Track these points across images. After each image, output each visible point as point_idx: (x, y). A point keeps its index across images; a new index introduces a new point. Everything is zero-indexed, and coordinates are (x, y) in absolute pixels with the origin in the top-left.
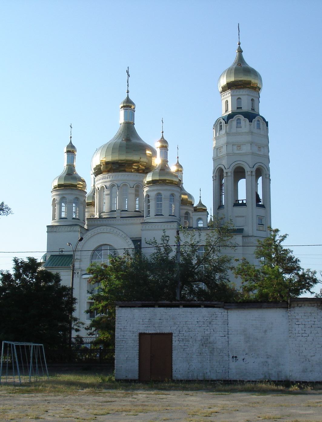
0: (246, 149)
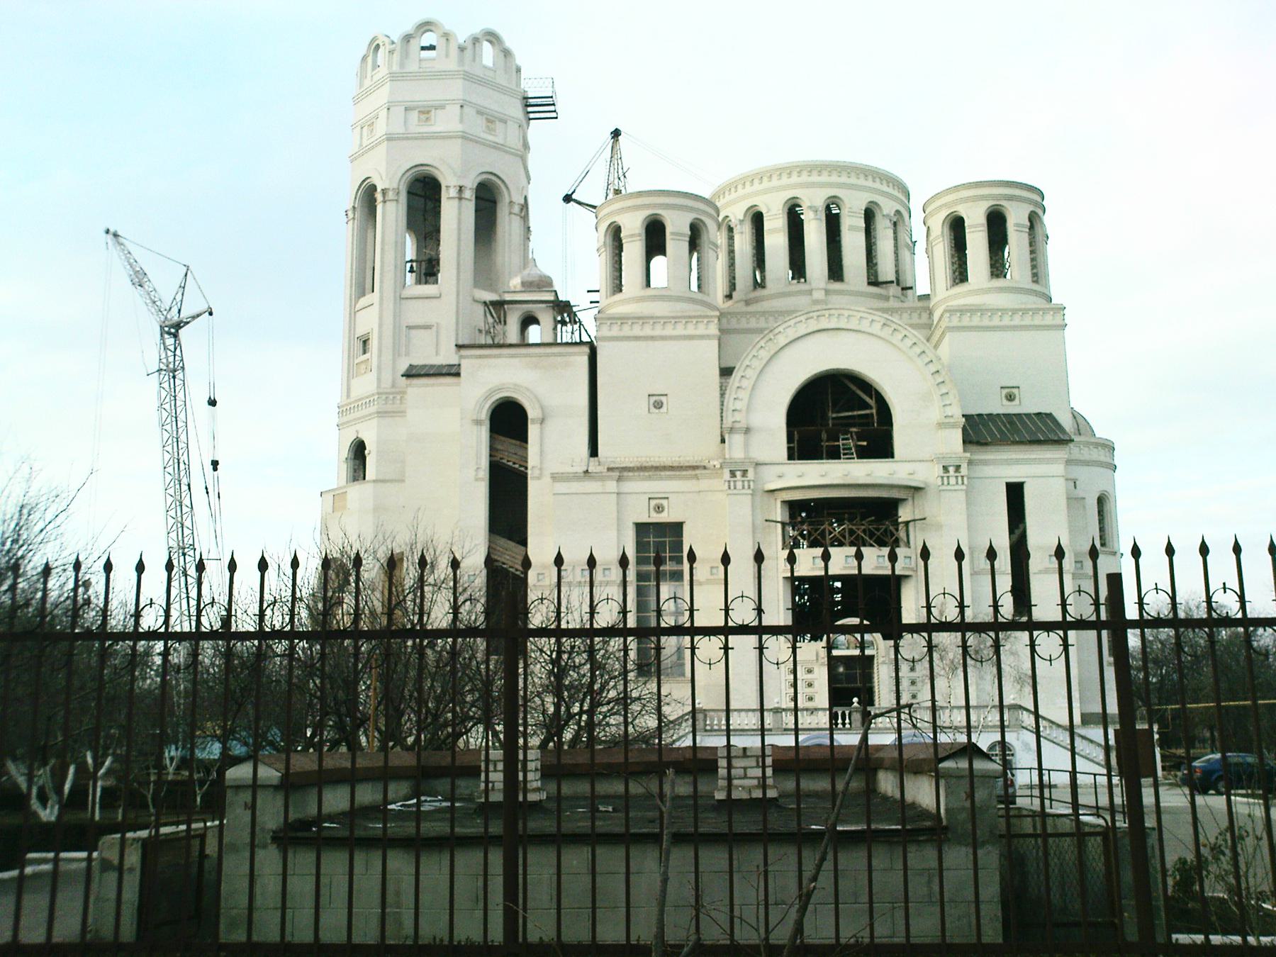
0: (447, 121)
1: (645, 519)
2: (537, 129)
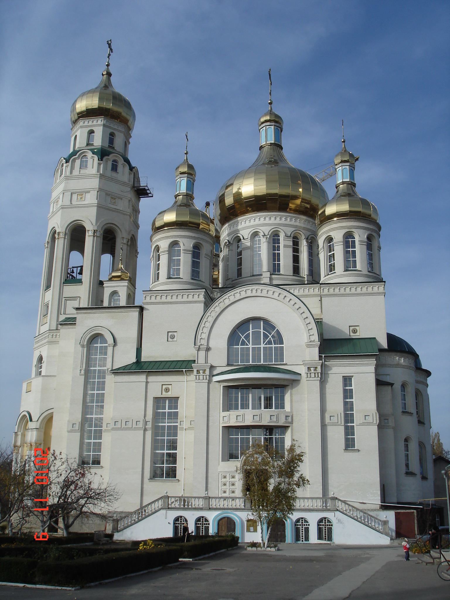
1: (159, 395)
2: (143, 201)
